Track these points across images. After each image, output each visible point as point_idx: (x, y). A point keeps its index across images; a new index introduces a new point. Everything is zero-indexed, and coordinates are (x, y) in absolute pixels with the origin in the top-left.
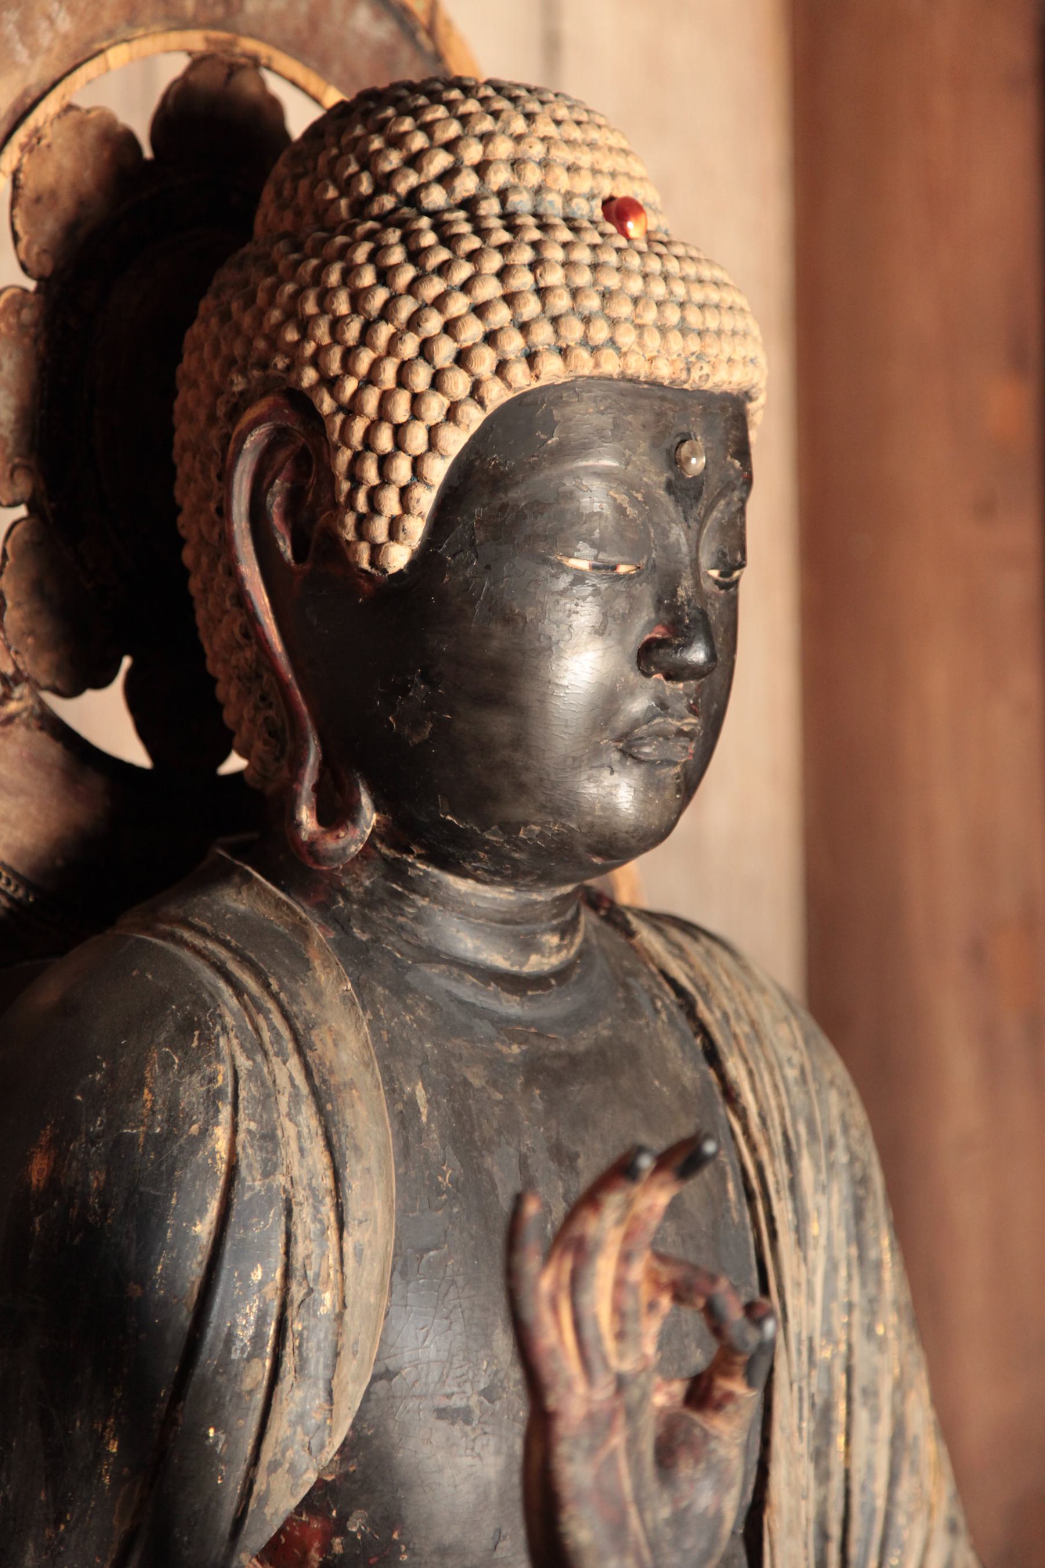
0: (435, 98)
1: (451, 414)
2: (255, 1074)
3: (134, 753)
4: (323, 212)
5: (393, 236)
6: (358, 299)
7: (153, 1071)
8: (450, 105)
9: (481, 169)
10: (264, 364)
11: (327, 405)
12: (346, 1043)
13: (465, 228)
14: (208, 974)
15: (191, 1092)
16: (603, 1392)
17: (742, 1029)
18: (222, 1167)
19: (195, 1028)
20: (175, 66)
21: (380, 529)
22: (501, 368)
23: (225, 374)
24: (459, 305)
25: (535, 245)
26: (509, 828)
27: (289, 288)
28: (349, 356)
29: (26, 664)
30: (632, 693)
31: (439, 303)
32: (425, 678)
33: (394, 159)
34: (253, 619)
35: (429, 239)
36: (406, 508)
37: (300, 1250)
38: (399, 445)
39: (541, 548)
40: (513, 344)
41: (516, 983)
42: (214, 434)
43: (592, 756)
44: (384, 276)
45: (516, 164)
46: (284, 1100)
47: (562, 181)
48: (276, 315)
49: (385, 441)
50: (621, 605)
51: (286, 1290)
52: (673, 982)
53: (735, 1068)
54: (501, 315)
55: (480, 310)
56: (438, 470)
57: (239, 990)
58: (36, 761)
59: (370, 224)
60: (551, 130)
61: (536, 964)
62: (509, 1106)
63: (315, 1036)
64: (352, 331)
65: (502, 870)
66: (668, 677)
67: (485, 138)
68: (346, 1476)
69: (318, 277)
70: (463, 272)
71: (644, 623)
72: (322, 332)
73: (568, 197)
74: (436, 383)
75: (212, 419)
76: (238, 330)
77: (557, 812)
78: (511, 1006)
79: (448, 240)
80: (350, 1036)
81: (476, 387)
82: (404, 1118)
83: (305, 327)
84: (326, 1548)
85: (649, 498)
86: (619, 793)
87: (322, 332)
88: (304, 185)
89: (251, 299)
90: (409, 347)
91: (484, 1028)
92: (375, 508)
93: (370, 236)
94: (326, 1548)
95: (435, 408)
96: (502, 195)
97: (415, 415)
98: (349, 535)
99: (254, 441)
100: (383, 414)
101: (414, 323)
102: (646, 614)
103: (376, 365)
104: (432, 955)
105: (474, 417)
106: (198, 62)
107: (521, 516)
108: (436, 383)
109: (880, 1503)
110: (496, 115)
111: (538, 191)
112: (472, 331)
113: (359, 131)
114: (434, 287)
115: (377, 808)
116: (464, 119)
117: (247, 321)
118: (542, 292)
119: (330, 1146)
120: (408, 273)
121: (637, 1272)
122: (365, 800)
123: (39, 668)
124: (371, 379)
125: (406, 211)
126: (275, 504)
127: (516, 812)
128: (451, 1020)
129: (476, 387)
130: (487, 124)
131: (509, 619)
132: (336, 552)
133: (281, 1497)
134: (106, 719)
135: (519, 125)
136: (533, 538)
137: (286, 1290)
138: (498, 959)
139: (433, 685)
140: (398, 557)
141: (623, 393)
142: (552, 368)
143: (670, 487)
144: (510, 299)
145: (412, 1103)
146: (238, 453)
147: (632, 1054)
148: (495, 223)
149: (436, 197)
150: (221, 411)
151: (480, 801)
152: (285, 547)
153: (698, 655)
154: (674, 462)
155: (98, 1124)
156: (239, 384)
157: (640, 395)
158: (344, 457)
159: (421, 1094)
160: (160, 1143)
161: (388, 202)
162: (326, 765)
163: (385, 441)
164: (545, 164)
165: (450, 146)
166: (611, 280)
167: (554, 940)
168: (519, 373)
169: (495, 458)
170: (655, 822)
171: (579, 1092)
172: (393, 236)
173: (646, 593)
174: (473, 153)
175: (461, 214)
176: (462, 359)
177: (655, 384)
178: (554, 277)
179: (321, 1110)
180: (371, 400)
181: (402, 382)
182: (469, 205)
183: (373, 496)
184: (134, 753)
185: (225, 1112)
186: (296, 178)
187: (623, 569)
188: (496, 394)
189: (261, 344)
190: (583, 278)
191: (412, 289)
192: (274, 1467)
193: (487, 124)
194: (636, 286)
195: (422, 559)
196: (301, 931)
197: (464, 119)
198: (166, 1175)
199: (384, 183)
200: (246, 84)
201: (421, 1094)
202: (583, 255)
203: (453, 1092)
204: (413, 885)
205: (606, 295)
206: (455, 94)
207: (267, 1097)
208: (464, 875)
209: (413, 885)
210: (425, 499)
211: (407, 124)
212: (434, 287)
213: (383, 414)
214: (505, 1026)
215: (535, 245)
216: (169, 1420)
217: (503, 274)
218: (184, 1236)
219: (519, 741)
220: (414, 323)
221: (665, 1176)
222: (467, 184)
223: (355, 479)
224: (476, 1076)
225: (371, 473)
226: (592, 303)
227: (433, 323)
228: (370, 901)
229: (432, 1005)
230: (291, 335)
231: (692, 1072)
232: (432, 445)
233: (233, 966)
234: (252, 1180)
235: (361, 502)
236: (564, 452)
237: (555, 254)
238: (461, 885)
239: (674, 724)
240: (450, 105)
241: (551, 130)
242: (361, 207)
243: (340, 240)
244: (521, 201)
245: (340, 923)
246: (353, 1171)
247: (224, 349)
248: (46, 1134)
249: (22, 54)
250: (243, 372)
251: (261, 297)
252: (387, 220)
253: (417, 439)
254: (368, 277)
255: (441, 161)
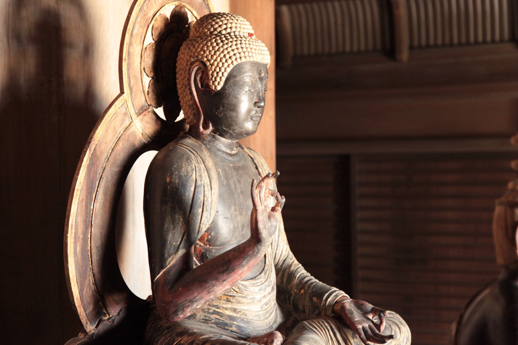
0: (222, 17)
1: (228, 66)
2: (198, 166)
3: (165, 119)
4: (205, 33)
5: (218, 38)
6: (213, 48)
7: (184, 165)
8: (225, 17)
9: (231, 28)
10: (197, 57)
11: (208, 64)
12: (210, 163)
13: (229, 37)
14: (189, 152)
15: (189, 169)
16: (263, 207)
17: (260, 164)
18: (194, 180)
19: (188, 159)
20: (174, 7)
21: (216, 83)
22: (236, 59)
23: (189, 58)
24: (230, 49)
25: (240, 40)
26: (234, 130)
27: (202, 45)
28: (212, 56)
29: (152, 104)
30: (253, 110)
31: (227, 49)
32: (222, 107)
33: (217, 26)
34: (194, 97)
35: (224, 39)
36: (221, 80)
37: (206, 193)
38: (220, 70)
39: (241, 87)
40: (238, 56)
41: (231, 155)
42: (187, 68)
43: (246, 120)
44: (217, 44)
45: (236, 27)
46: (202, 170)
47: (242, 30)
48: (199, 49)
49: (218, 70)
50: (252, 96)
51: (204, 198)
52: (250, 157)
53: (260, 170)
54: (236, 51)
55: (233, 50)
56: (226, 75)
57: (194, 154)
58: (152, 118)
59: (214, 36)
60: (240, 22)
61: (234, 152)
62: (232, 174)
63: (206, 161)
64: (213, 53)
65: (231, 137)
66: (258, 107)
67: (231, 23)
68: (211, 227)
69: (206, 44)
70: (230, 44)
71: (255, 99)
72: (208, 52)
73: (244, 33)
74: (226, 61)
75: (187, 65)
76: (192, 51)
77: (241, 128)
78: (230, 158)
79: (227, 39)
80: (210, 161)
81: (232, 62)
82: (218, 174)
83: (204, 51)
84: (208, 237)
85: (256, 80)
86: (249, 126)
87: (208, 52)
88: (201, 29)
89: (194, 47)
90: (222, 55)
91: (227, 162)
92: (216, 80)
93: (214, 38)
94: (208, 237)
95: (226, 65)
96: (234, 32)
97: (223, 66)
98: (211, 84)
99: (195, 69)
100: (218, 66)
101: (223, 52)
102: (255, 98)
103: (217, 58)
104: (219, 150)
105: (232, 67)
106: (176, 6)
107: (238, 82)
108: (226, 61)
109: (277, 240)
110: (232, 19)
111: (239, 32)
112: (232, 53)
113: (210, 21)
114: (226, 47)
115: (212, 127)
116: (227, 20)
117: (194, 50)
118: (242, 48)
119: (209, 177)
120: (221, 44)
121: (267, 192)
122: (211, 125)
123: (153, 103)
124: (215, 60)
125: (219, 34)
126: (198, 78)
127: (235, 128)
128: (223, 160)
129: (232, 62)
130: (231, 21)
131: (236, 98)
132: (208, 86)
133: (204, 228)
134: (160, 112)
135: (236, 21)
136: (240, 85)
137: (204, 198)
138: (228, 151)
139: (224, 108)
140: (219, 88)
141: (253, 64)
142: (244, 60)
143: (259, 78)
144: (237, 49)
145: (219, 172)
146: (193, 71)
147: (247, 167)
148: (234, 37)
149: (224, 32)
150: (189, 64)
151: (229, 126)
152: (200, 86)
153: (262, 104)
154: (260, 74)
155: (176, 173)
156: (193, 60)
157: (255, 64)
158: (211, 72)
159: (220, 171)
160: (186, 176)
161: (216, 32)
162: (204, 120)
163: (218, 70)
164: (240, 28)
165: (226, 24)
166: (252, 46)
167: (235, 149)
168: (239, 60)
169: (234, 73)
170: (255, 130)
171: (240, 172)
172: (218, 38)
173: (255, 94)
174: (229, 25)
175: (228, 35)
176: (230, 58)
177: (257, 62)
178: (243, 46)
179: (207, 172)
180: (216, 63)
181: (221, 61)
182: (229, 33)
183: (215, 78)
184: (165, 119)
185: (194, 172)
186: (199, 28)
187: (252, 91)
188: (235, 63)
189: (197, 54)
190: (248, 46)
191: (222, 46)
192: (203, 224)
193: (231, 21)
194: (255, 47)
195: (223, 88)
196: (200, 145)
197: (227, 20)
198: (187, 181)
199: (215, 29)
200: (183, 10)
201: (220, 171)
202: (247, 42)
203: (224, 170)
204: (216, 139)
205: (251, 48)
206: (225, 16)
207: (200, 170)
208: (224, 137)
209: (216, 139)
210: (224, 79)
211: (218, 20)
212: (226, 47)
213: (218, 66)
214: (230, 161)
215: (240, 40)
216: (189, 216)
217: (236, 45)
218: (190, 190)
219: (236, 117)
220: (223, 52)
221: (273, 177)
222: (229, 30)
223: (212, 75)
224: (227, 169)
225: (215, 75)
226: (249, 50)
227: (226, 52)
228: (210, 141)
229: (220, 158)
230: (202, 53)
231: (255, 170)
232: (225, 71)
233: (192, 150)
234: (199, 182)
235: (214, 79)
236: (244, 72)
237: (243, 42)
238: (223, 139)
239: (258, 115)
240: (225, 17)
241: (240, 22)
242: (211, 33)
243: (210, 38)
244: (237, 33)
245: (206, 145)
246: (212, 182)
247: (189, 54)
248: (169, 174)
249: (154, 6)
250: (193, 58)
251: (196, 46)
252: (216, 35)
253: (223, 70)
254: (215, 44)
255: (224, 26)
